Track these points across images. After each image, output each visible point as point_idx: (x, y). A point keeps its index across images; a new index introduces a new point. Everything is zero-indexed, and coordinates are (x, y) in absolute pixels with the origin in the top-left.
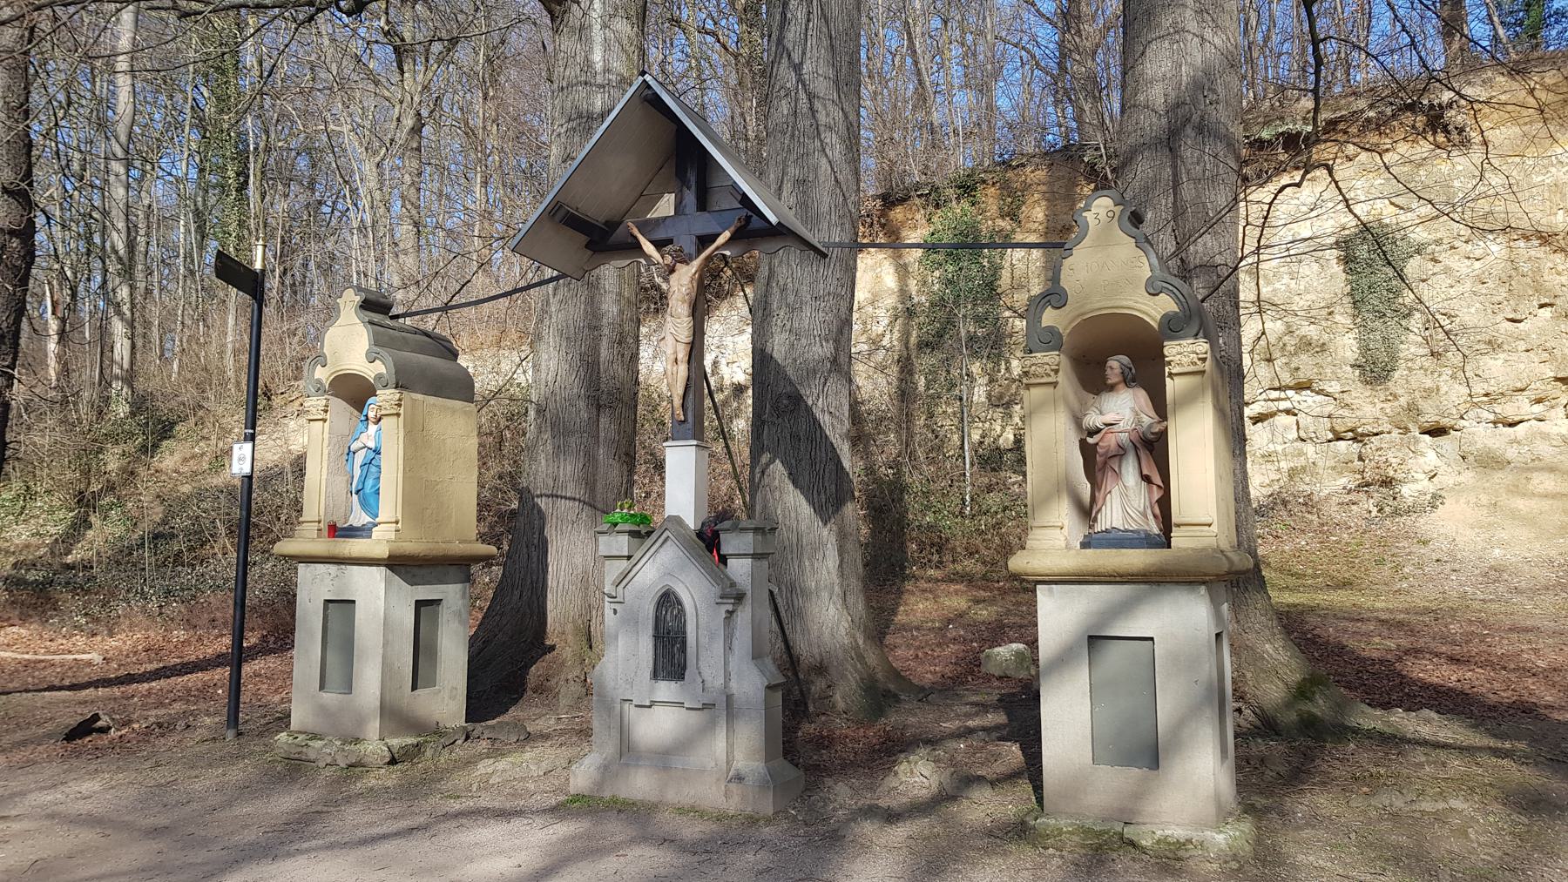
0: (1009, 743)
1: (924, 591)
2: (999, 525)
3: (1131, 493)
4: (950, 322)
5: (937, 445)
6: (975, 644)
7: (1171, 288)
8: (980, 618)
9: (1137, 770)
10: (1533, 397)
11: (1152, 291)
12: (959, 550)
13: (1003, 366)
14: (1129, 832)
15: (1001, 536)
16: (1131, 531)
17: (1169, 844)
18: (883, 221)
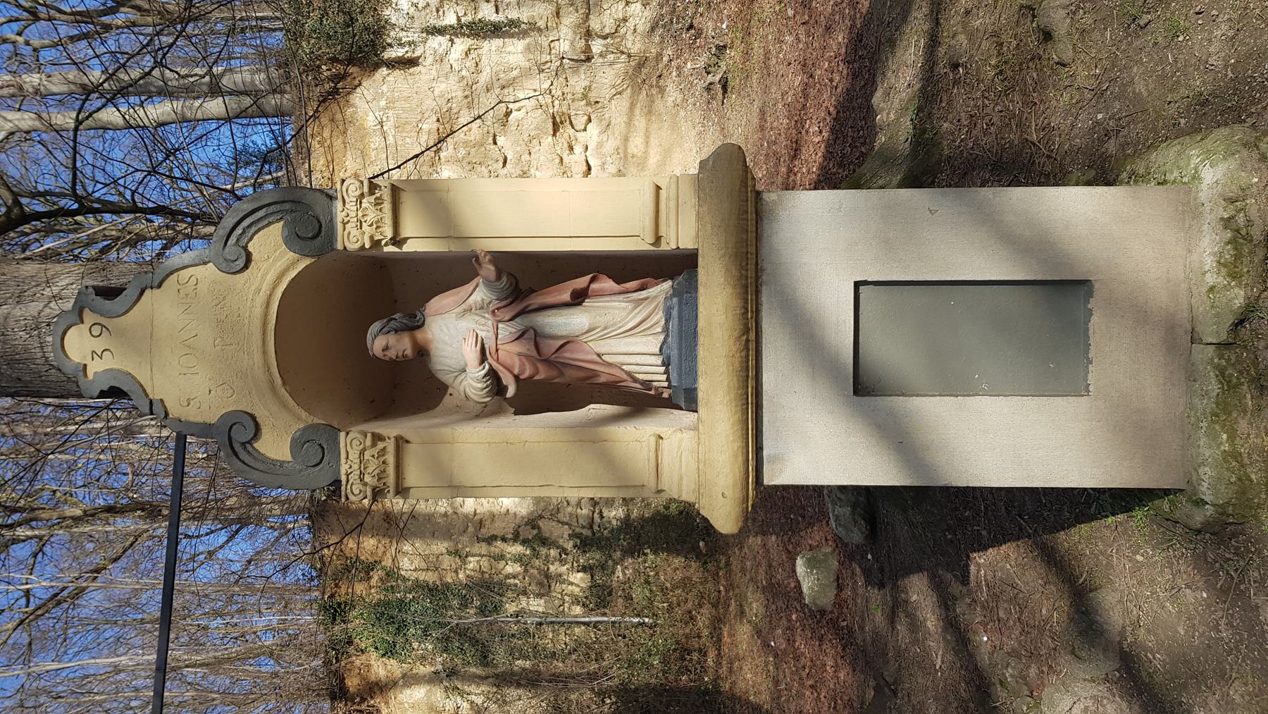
0: (973, 568)
1: (731, 670)
2: (663, 590)
3: (601, 320)
4: (463, 633)
5: (583, 649)
6: (794, 617)
7: (239, 231)
8: (762, 610)
9: (1094, 319)
10: (568, 152)
11: (241, 263)
12: (688, 631)
13: (511, 581)
14: (1214, 332)
15: (674, 588)
16: (667, 321)
17: (1238, 257)
18: (358, 700)
